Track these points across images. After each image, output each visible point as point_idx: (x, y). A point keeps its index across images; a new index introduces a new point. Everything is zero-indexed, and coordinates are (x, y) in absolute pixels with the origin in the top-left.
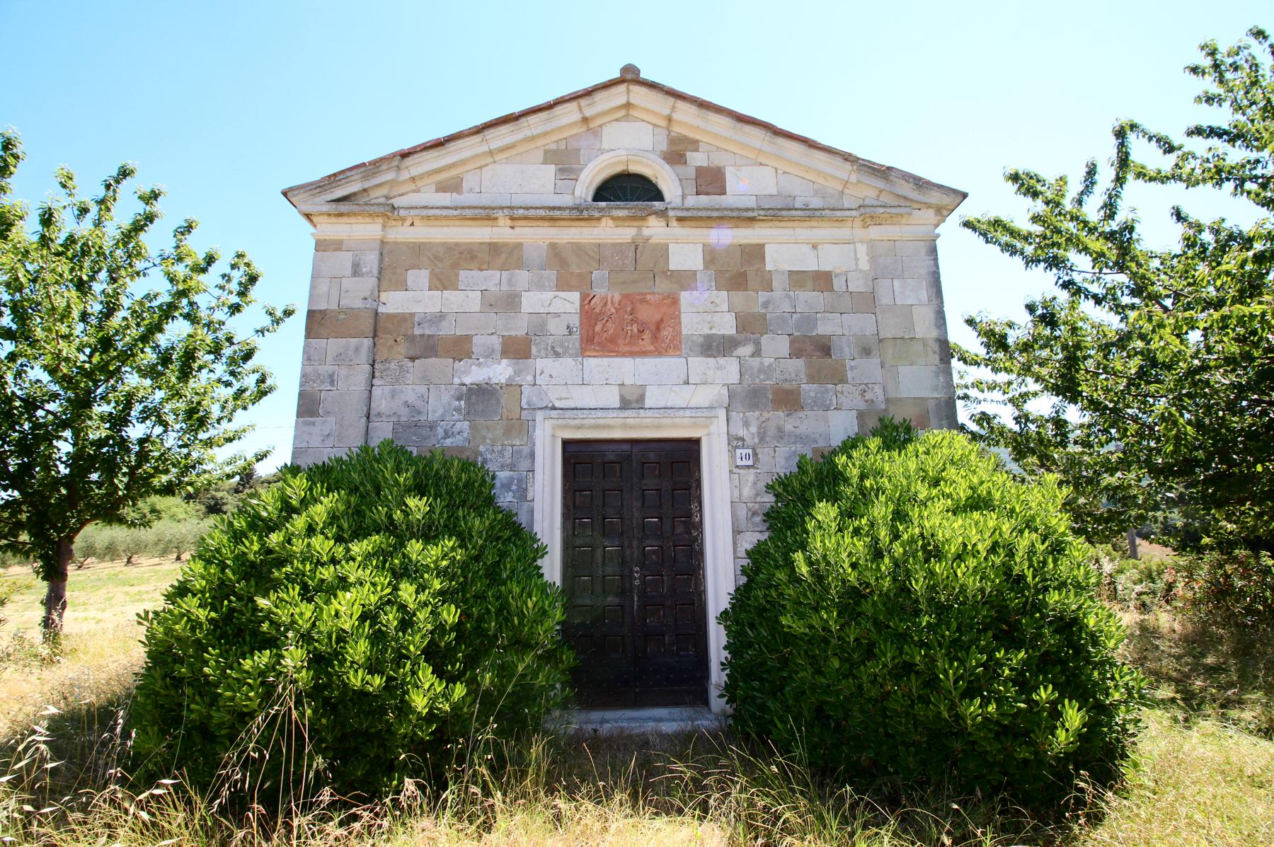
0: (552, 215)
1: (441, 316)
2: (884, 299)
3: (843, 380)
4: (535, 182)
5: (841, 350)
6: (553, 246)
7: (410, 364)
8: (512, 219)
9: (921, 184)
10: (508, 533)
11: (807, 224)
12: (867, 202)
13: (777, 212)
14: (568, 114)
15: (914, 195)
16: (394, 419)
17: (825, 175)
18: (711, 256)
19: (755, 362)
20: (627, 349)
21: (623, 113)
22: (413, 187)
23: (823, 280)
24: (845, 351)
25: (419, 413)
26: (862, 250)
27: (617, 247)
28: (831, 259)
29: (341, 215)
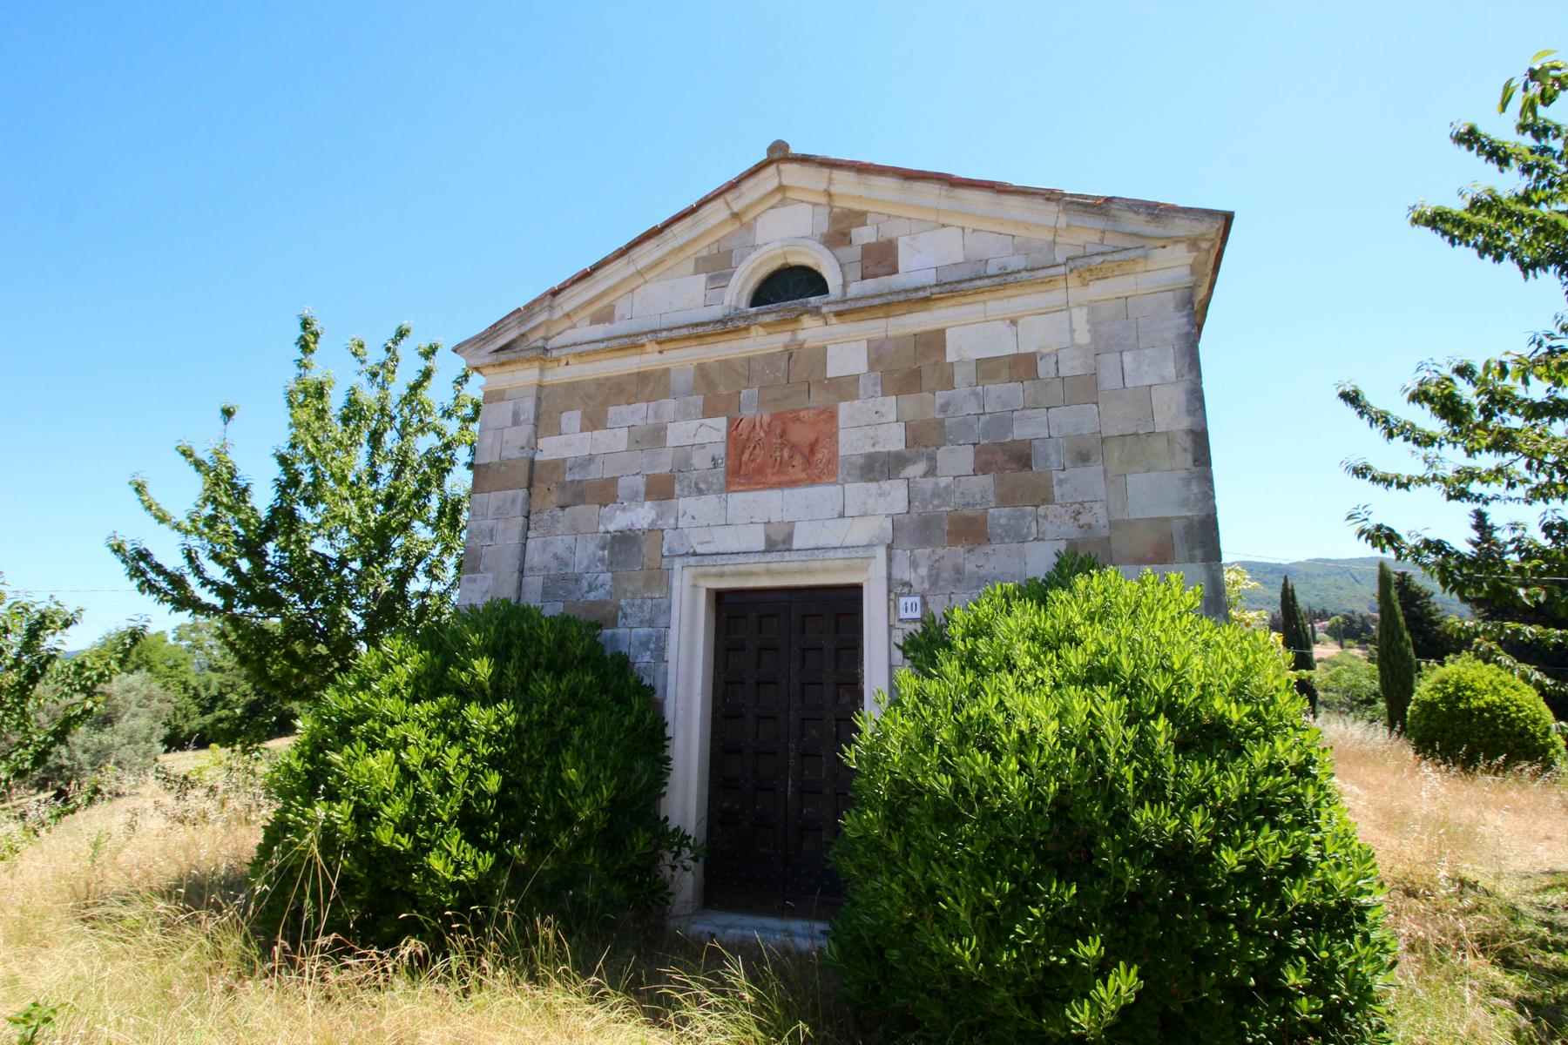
0: (698, 332)
1: (591, 459)
2: (1109, 381)
3: (1048, 500)
4: (682, 295)
5: (1047, 458)
6: (701, 368)
7: (560, 513)
8: (659, 343)
9: (1155, 211)
10: (1030, 679)
11: (1001, 294)
12: (1088, 251)
13: (953, 287)
14: (716, 213)
15: (1152, 229)
16: (544, 573)
17: (1027, 225)
18: (877, 355)
19: (928, 484)
20: (776, 479)
21: (778, 197)
22: (569, 323)
23: (1023, 366)
24: (1051, 459)
25: (567, 565)
26: (1080, 317)
27: (769, 358)
28: (1036, 336)
29: (502, 364)
